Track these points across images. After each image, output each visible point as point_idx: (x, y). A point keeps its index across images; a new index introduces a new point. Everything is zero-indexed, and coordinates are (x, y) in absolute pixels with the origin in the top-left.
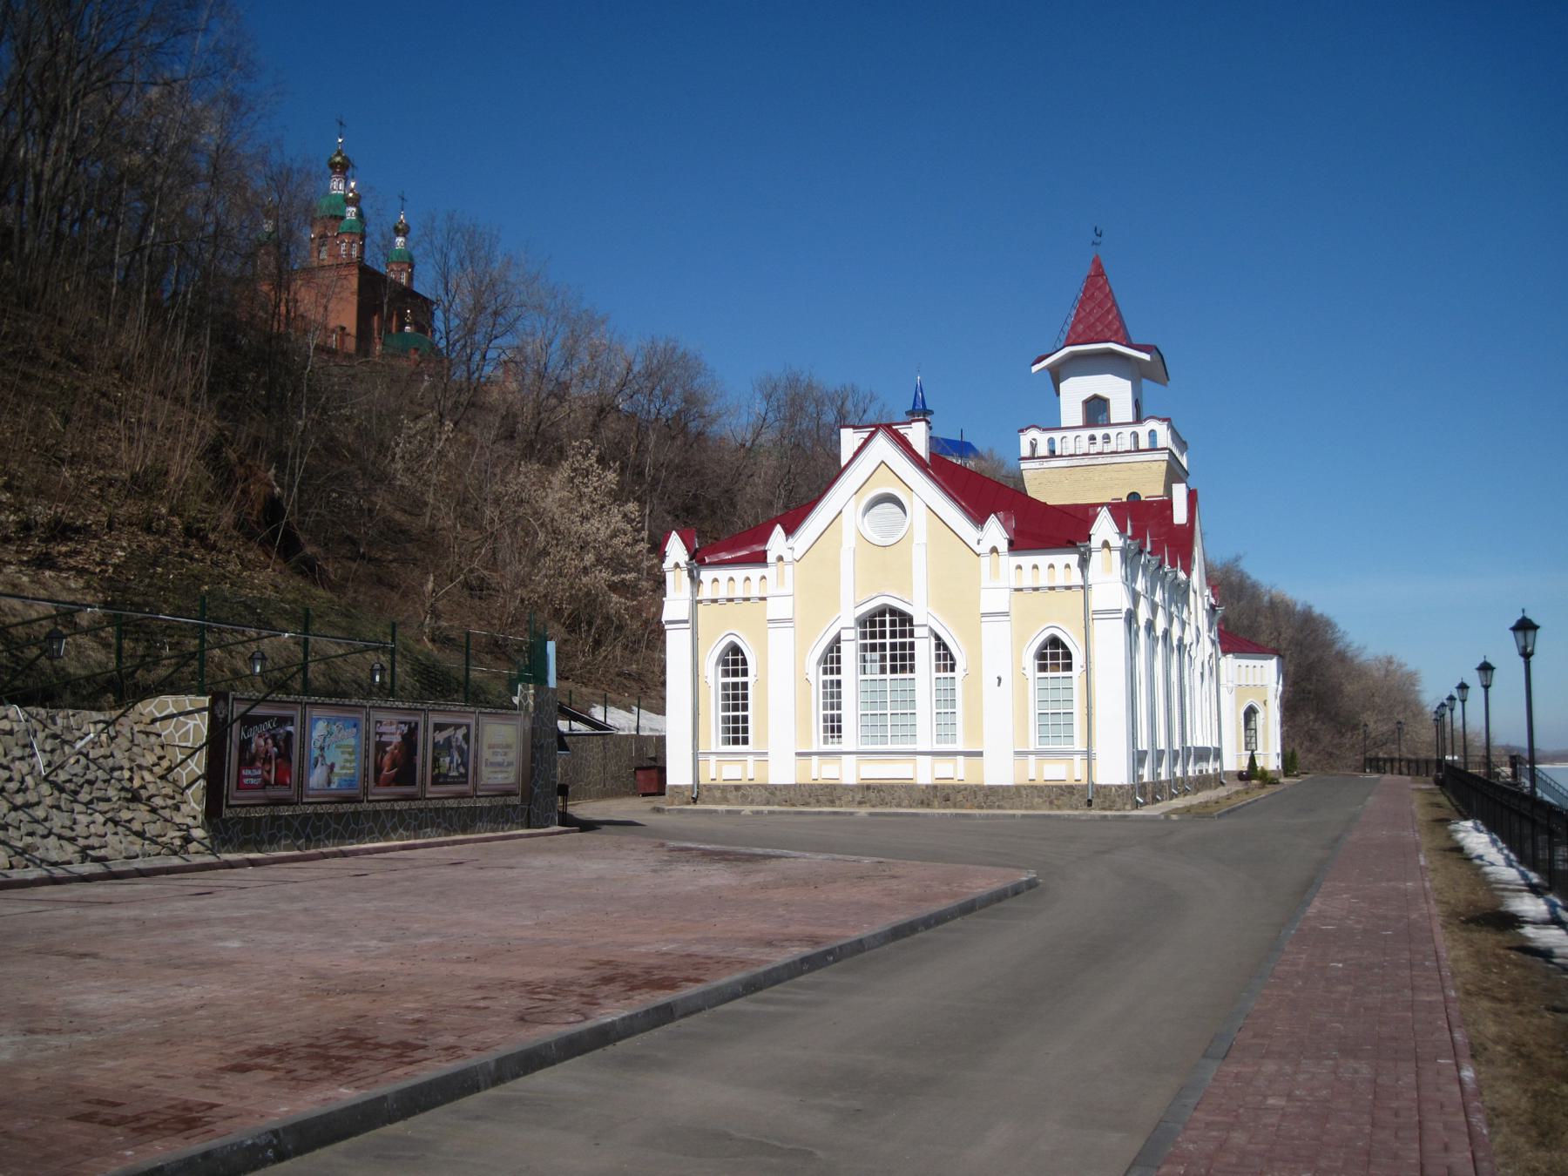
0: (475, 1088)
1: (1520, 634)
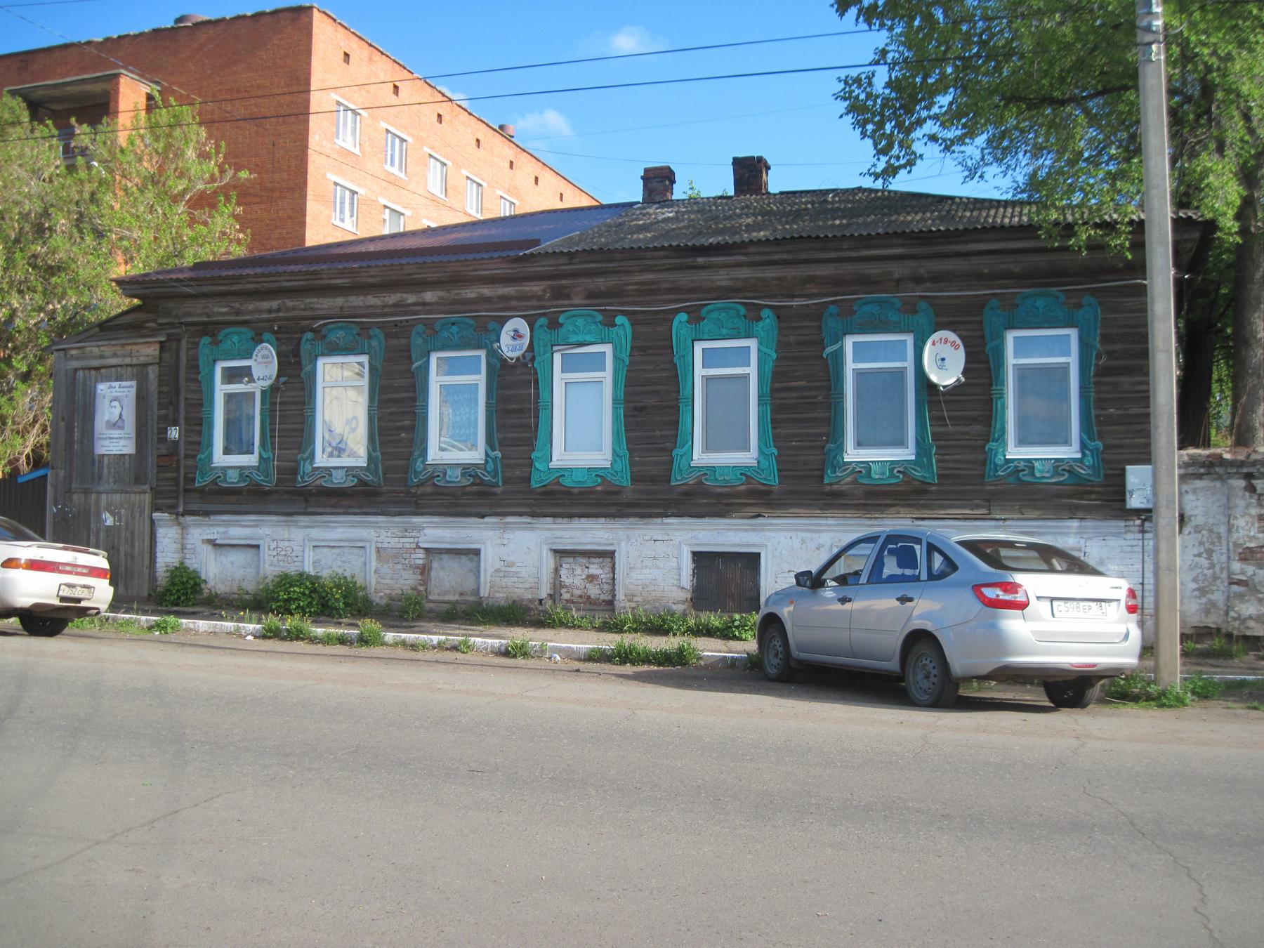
0: (52, 570)
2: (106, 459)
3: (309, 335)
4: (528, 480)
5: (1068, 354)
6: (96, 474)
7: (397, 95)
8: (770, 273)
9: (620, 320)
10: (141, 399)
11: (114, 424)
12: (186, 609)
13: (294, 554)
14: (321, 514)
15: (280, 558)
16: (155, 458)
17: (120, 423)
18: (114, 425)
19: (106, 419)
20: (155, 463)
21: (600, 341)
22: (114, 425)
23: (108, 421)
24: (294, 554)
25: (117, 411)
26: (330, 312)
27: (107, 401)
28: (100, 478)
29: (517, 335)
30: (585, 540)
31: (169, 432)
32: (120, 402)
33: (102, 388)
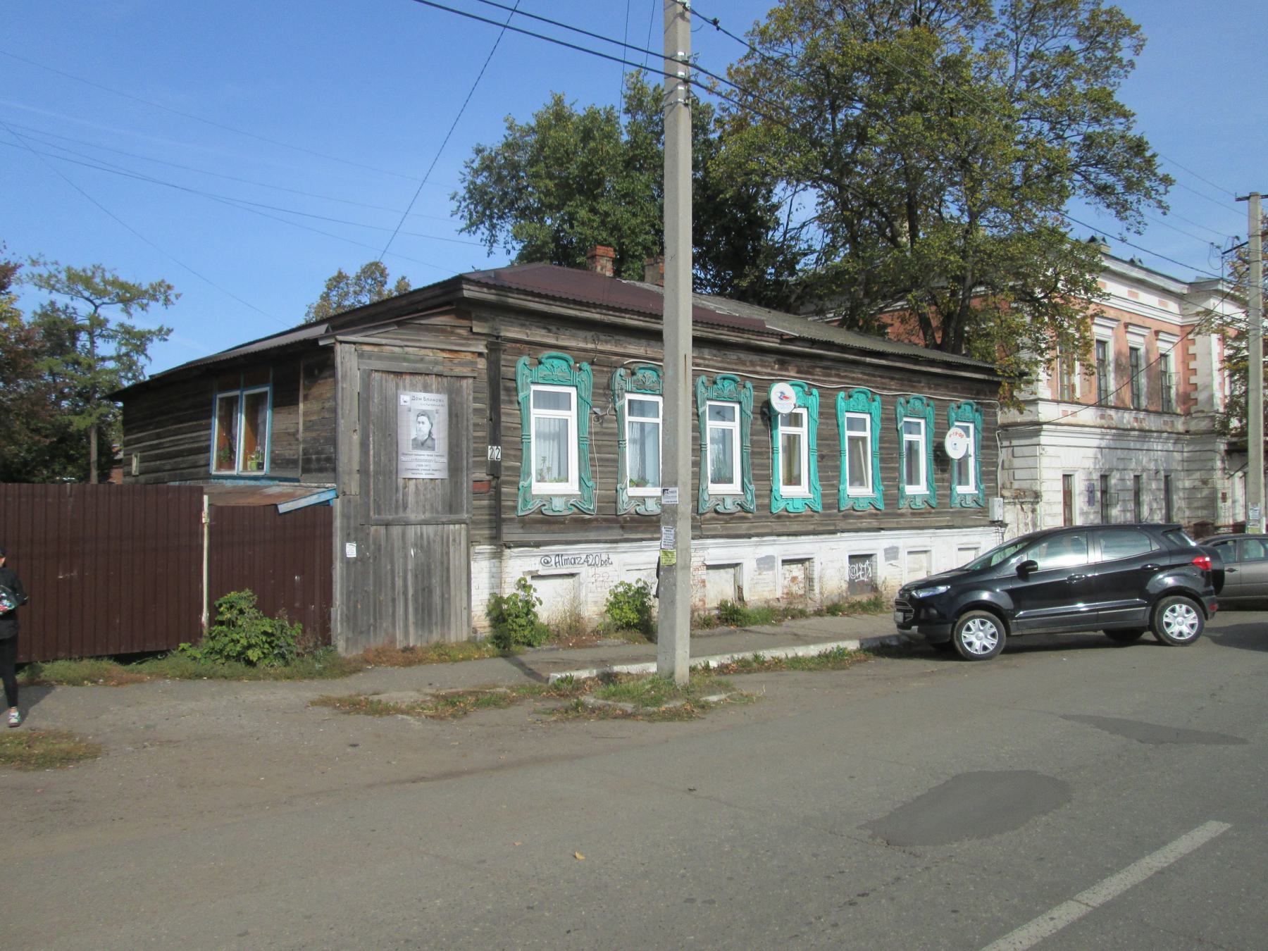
1: (510, 533)
2: (412, 484)
3: (622, 371)
4: (769, 506)
5: (865, 430)
6: (401, 501)
7: (1140, 26)
8: (865, 377)
9: (815, 391)
10: (454, 416)
11: (423, 444)
12: (437, 592)
13: (610, 579)
14: (642, 540)
15: (598, 584)
16: (471, 483)
17: (429, 443)
18: (421, 445)
19: (413, 437)
20: (471, 489)
21: (569, 383)
22: (421, 445)
23: (415, 440)
24: (610, 579)
25: (425, 428)
26: (743, 356)
27: (412, 416)
28: (405, 508)
29: (783, 397)
30: (800, 552)
31: (490, 452)
32: (429, 418)
33: (405, 398)
